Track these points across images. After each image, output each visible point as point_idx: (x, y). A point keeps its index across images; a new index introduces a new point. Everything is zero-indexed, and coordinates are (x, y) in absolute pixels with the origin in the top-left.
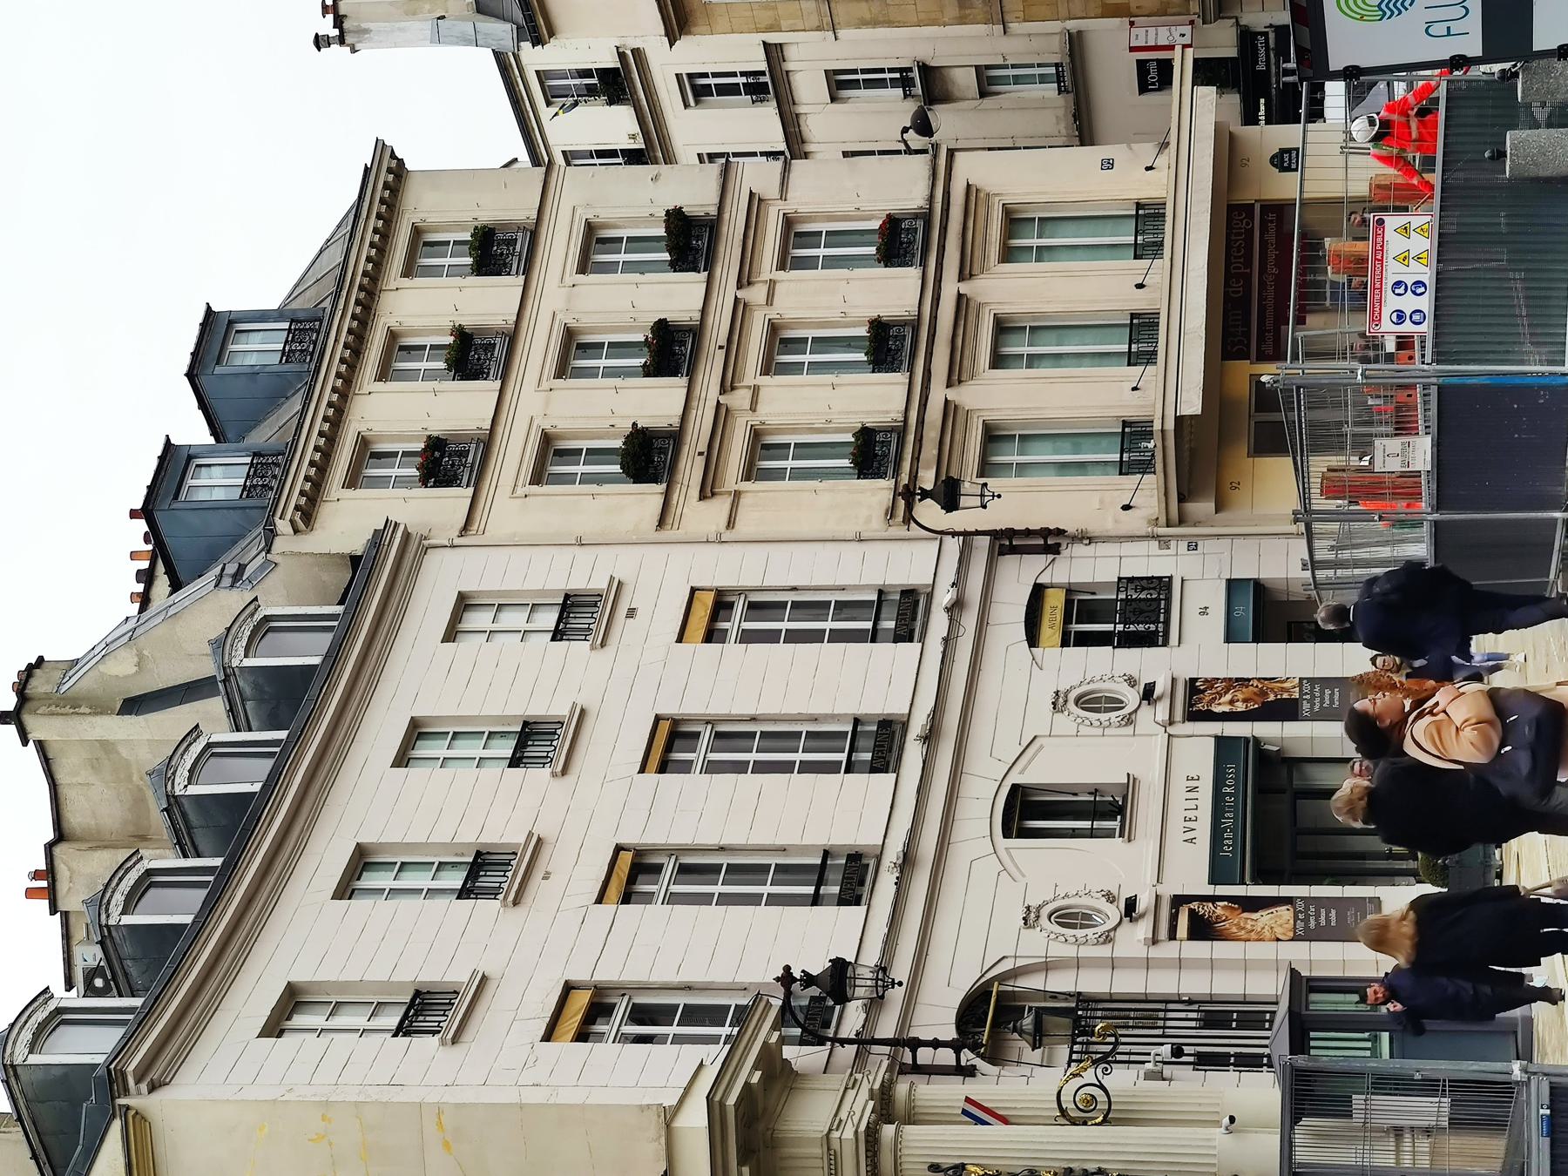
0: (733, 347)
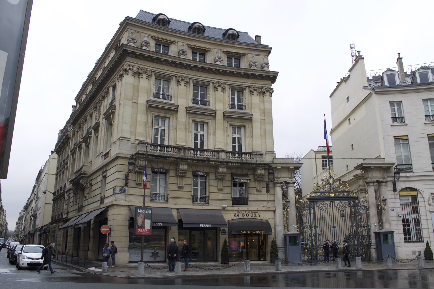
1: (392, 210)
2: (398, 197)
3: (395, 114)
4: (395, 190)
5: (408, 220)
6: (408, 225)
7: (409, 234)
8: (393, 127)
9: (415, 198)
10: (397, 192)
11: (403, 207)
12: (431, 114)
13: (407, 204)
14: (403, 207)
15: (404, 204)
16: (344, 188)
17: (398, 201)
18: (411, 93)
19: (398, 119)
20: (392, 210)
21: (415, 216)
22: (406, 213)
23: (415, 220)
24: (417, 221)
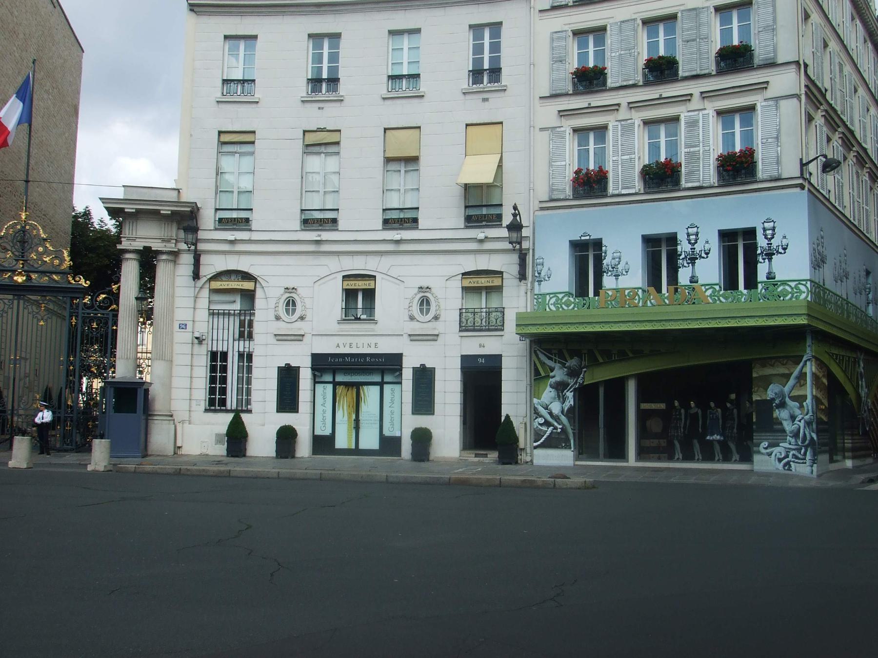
0: (590, 110)
1: (183, 326)
2: (205, 293)
3: (320, 69)
4: (196, 276)
5: (224, 355)
6: (224, 369)
7: (223, 391)
8: (468, 97)
9: (249, 296)
10: (203, 280)
11: (216, 320)
12: (405, 73)
13: (227, 314)
14: (216, 320)
15: (229, 314)
16: (57, 262)
17: (203, 303)
18: (283, 13)
19: (324, 83)
20: (183, 326)
21: (242, 346)
22: (220, 338)
23: (241, 355)
24: (247, 358)
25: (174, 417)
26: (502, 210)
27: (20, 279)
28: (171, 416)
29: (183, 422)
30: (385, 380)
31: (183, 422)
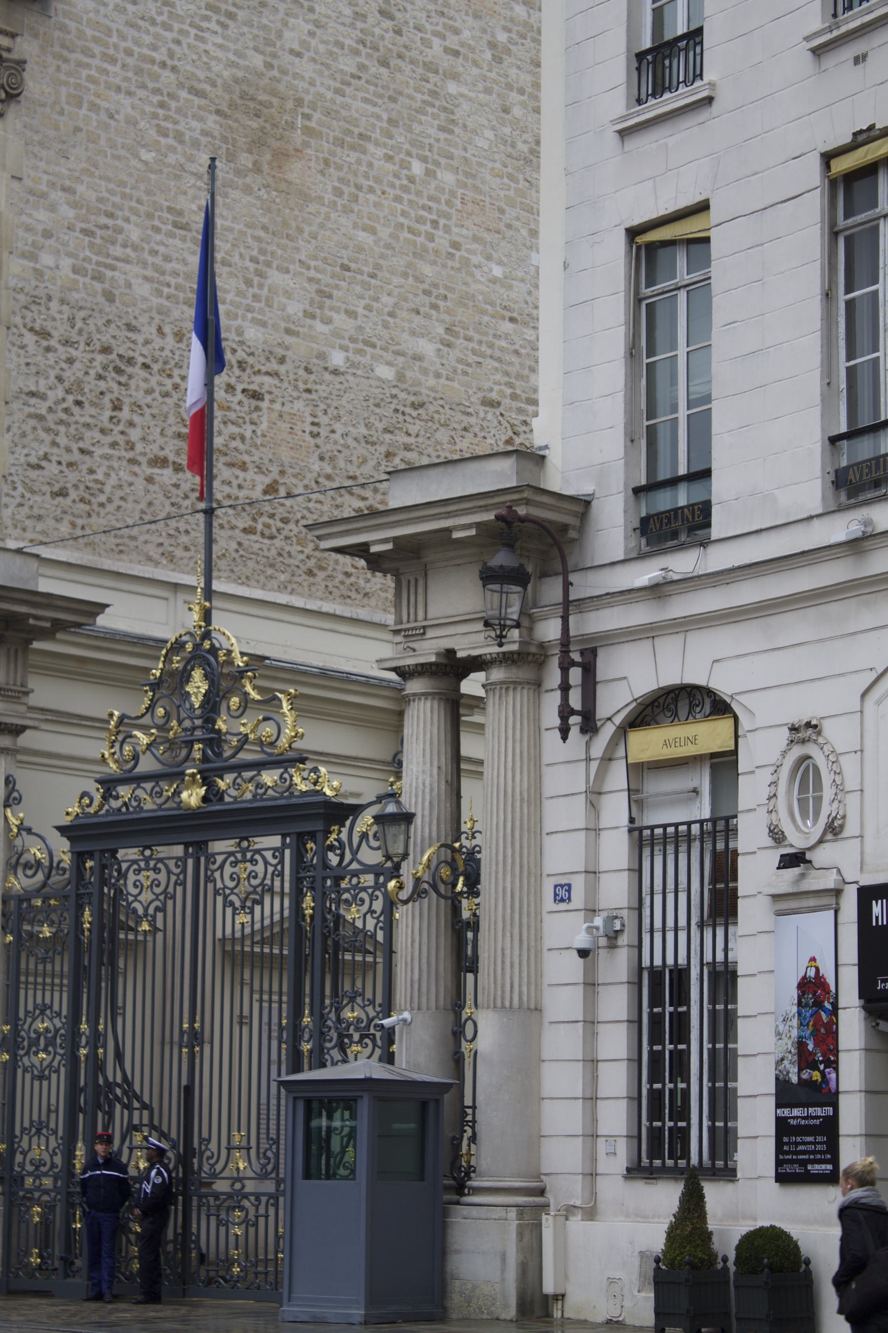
5: (681, 975)
10: (608, 731)
17: (616, 810)
24: (724, 980)
25: (550, 1197)
26: (710, 492)
27: (192, 797)
28: (542, 1192)
29: (569, 1211)
30: (470, 1104)
31: (569, 1211)
